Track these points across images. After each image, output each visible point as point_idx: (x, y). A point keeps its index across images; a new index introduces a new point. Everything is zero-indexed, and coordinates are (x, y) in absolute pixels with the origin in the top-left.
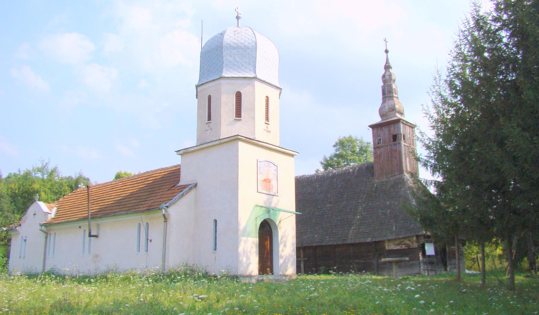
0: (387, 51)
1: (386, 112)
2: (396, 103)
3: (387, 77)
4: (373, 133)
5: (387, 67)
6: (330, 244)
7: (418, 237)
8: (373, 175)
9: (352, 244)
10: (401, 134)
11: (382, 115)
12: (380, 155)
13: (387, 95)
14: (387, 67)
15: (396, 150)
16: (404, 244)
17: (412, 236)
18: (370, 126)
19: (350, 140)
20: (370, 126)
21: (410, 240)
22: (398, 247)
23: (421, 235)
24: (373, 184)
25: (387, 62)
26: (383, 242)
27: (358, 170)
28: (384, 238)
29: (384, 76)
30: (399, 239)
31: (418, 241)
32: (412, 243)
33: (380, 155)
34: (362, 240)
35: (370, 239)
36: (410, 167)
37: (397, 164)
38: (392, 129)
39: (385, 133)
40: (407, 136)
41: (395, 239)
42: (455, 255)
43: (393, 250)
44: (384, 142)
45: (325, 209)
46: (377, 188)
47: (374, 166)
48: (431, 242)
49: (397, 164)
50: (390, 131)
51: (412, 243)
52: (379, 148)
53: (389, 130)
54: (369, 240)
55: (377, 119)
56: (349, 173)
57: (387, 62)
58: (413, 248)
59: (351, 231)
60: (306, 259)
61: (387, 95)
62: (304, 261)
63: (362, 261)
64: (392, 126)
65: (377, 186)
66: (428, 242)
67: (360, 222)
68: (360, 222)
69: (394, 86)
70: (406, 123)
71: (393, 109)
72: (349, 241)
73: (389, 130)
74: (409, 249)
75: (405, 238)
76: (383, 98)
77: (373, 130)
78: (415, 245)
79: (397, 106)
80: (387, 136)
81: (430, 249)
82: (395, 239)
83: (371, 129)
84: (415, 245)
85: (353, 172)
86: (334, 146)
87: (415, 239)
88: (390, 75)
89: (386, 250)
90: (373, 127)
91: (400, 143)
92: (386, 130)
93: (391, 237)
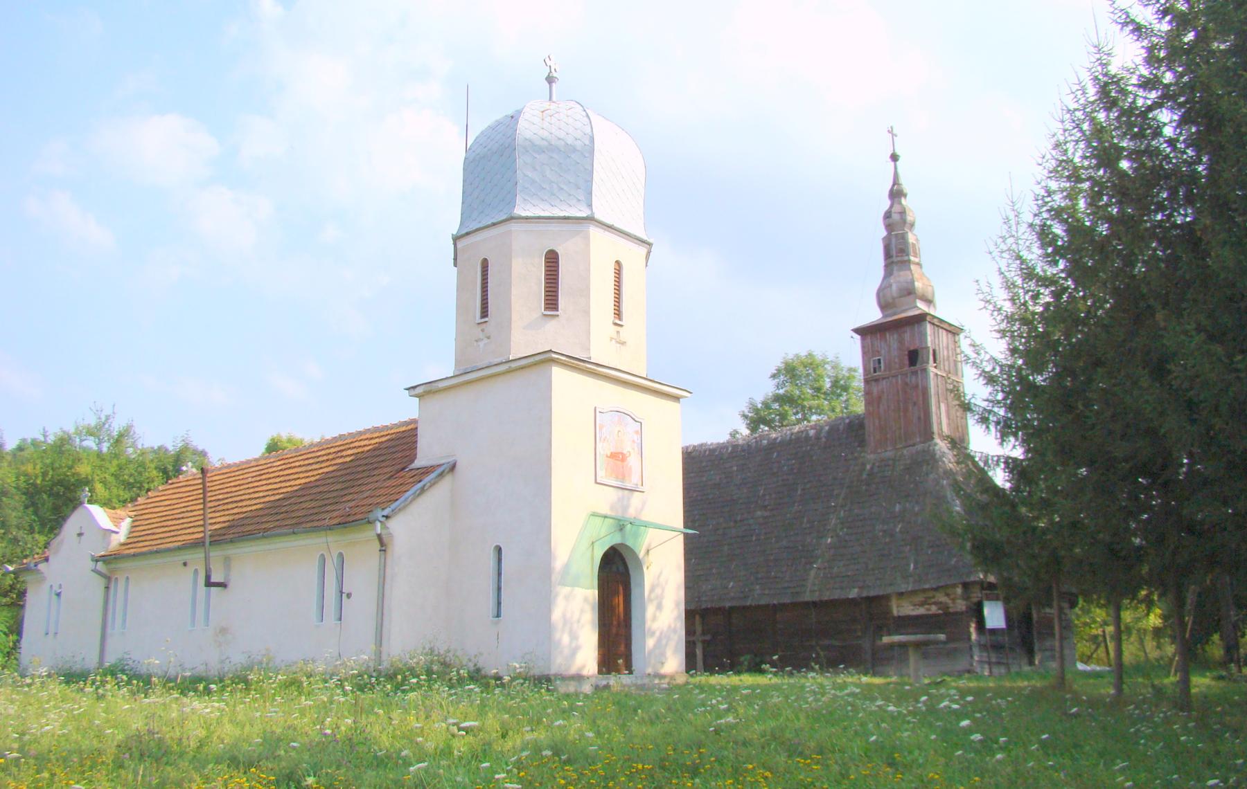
0: (894, 158)
1: (894, 299)
2: (916, 276)
3: (896, 217)
4: (863, 347)
5: (896, 194)
6: (762, 602)
7: (966, 586)
8: (862, 443)
9: (814, 604)
10: (927, 348)
11: (884, 306)
12: (880, 398)
13: (895, 259)
14: (896, 194)
15: (917, 386)
16: (935, 603)
17: (954, 586)
18: (857, 331)
19: (811, 364)
20: (857, 331)
21: (947, 595)
22: (921, 611)
23: (974, 583)
24: (864, 465)
25: (896, 181)
26: (886, 598)
27: (829, 432)
28: (889, 590)
29: (888, 215)
30: (924, 591)
31: (966, 597)
32: (953, 600)
33: (880, 398)
34: (837, 595)
35: (856, 590)
36: (949, 424)
37: (919, 418)
38: (907, 336)
39: (891, 346)
40: (942, 353)
41: (913, 592)
42: (1052, 628)
43: (909, 618)
44: (888, 367)
45: (751, 521)
46: (871, 474)
47: (866, 421)
48: (997, 599)
49: (919, 418)
50: (901, 342)
51: (953, 600)
52: (877, 380)
53: (900, 338)
54: (853, 593)
55: (873, 315)
56: (807, 438)
57: (896, 181)
58: (956, 613)
59: (812, 573)
60: (708, 637)
61: (895, 259)
62: (704, 642)
63: (837, 643)
64: (908, 329)
65: (872, 468)
66: (989, 598)
67: (832, 551)
68: (832, 551)
69: (911, 238)
70: (940, 324)
71: (909, 292)
72: (807, 597)
73: (900, 338)
74: (947, 614)
75: (936, 589)
76: (886, 266)
77: (863, 339)
78: (961, 605)
79: (918, 285)
80: (895, 353)
81: (994, 616)
82: (913, 592)
83: (858, 337)
84: (961, 605)
85: (817, 437)
86: (774, 376)
87: (959, 590)
88: (903, 213)
89: (894, 618)
90: (863, 332)
91: (925, 370)
92: (892, 339)
93: (904, 587)
